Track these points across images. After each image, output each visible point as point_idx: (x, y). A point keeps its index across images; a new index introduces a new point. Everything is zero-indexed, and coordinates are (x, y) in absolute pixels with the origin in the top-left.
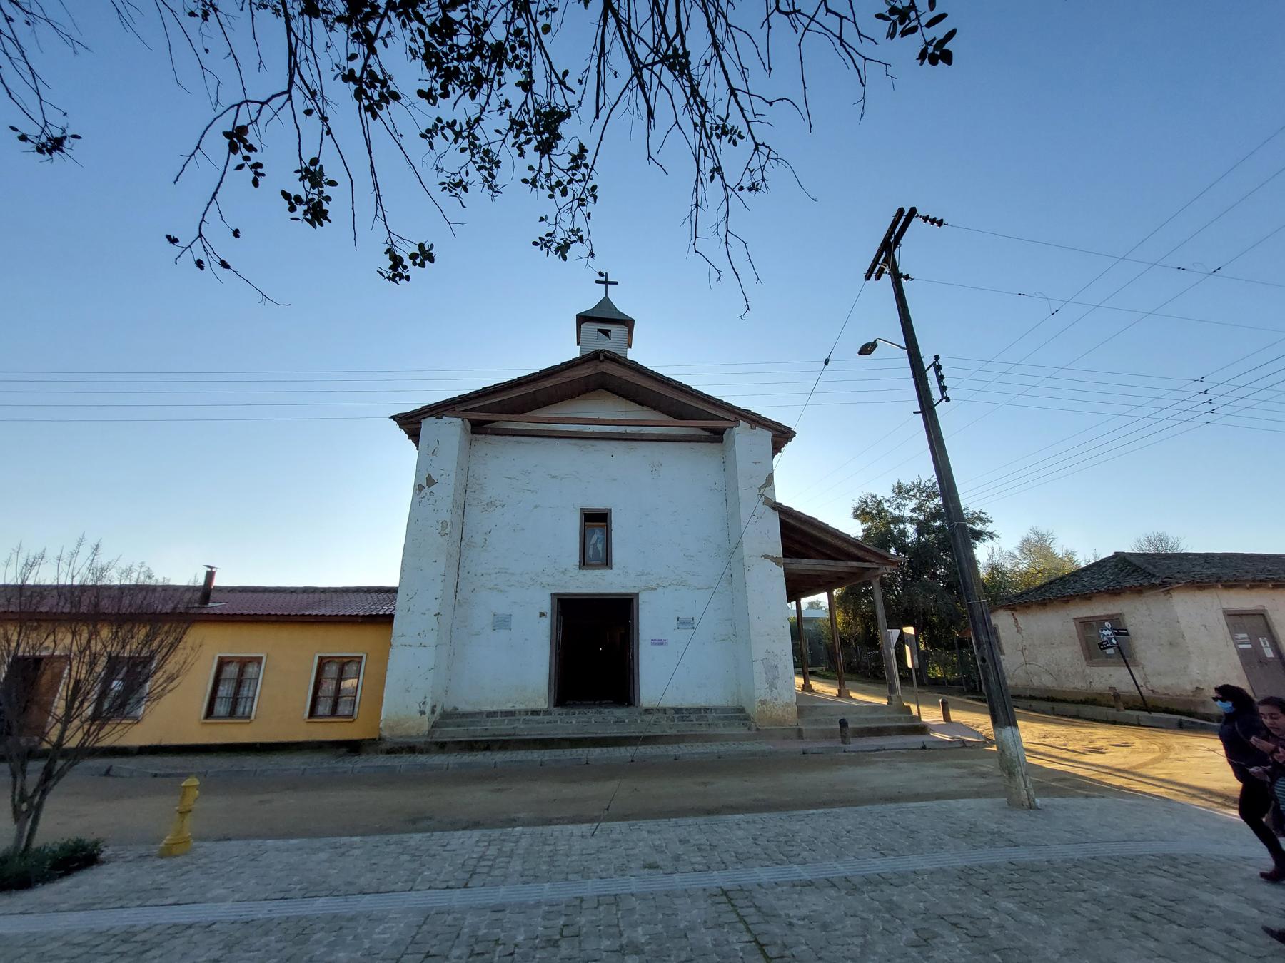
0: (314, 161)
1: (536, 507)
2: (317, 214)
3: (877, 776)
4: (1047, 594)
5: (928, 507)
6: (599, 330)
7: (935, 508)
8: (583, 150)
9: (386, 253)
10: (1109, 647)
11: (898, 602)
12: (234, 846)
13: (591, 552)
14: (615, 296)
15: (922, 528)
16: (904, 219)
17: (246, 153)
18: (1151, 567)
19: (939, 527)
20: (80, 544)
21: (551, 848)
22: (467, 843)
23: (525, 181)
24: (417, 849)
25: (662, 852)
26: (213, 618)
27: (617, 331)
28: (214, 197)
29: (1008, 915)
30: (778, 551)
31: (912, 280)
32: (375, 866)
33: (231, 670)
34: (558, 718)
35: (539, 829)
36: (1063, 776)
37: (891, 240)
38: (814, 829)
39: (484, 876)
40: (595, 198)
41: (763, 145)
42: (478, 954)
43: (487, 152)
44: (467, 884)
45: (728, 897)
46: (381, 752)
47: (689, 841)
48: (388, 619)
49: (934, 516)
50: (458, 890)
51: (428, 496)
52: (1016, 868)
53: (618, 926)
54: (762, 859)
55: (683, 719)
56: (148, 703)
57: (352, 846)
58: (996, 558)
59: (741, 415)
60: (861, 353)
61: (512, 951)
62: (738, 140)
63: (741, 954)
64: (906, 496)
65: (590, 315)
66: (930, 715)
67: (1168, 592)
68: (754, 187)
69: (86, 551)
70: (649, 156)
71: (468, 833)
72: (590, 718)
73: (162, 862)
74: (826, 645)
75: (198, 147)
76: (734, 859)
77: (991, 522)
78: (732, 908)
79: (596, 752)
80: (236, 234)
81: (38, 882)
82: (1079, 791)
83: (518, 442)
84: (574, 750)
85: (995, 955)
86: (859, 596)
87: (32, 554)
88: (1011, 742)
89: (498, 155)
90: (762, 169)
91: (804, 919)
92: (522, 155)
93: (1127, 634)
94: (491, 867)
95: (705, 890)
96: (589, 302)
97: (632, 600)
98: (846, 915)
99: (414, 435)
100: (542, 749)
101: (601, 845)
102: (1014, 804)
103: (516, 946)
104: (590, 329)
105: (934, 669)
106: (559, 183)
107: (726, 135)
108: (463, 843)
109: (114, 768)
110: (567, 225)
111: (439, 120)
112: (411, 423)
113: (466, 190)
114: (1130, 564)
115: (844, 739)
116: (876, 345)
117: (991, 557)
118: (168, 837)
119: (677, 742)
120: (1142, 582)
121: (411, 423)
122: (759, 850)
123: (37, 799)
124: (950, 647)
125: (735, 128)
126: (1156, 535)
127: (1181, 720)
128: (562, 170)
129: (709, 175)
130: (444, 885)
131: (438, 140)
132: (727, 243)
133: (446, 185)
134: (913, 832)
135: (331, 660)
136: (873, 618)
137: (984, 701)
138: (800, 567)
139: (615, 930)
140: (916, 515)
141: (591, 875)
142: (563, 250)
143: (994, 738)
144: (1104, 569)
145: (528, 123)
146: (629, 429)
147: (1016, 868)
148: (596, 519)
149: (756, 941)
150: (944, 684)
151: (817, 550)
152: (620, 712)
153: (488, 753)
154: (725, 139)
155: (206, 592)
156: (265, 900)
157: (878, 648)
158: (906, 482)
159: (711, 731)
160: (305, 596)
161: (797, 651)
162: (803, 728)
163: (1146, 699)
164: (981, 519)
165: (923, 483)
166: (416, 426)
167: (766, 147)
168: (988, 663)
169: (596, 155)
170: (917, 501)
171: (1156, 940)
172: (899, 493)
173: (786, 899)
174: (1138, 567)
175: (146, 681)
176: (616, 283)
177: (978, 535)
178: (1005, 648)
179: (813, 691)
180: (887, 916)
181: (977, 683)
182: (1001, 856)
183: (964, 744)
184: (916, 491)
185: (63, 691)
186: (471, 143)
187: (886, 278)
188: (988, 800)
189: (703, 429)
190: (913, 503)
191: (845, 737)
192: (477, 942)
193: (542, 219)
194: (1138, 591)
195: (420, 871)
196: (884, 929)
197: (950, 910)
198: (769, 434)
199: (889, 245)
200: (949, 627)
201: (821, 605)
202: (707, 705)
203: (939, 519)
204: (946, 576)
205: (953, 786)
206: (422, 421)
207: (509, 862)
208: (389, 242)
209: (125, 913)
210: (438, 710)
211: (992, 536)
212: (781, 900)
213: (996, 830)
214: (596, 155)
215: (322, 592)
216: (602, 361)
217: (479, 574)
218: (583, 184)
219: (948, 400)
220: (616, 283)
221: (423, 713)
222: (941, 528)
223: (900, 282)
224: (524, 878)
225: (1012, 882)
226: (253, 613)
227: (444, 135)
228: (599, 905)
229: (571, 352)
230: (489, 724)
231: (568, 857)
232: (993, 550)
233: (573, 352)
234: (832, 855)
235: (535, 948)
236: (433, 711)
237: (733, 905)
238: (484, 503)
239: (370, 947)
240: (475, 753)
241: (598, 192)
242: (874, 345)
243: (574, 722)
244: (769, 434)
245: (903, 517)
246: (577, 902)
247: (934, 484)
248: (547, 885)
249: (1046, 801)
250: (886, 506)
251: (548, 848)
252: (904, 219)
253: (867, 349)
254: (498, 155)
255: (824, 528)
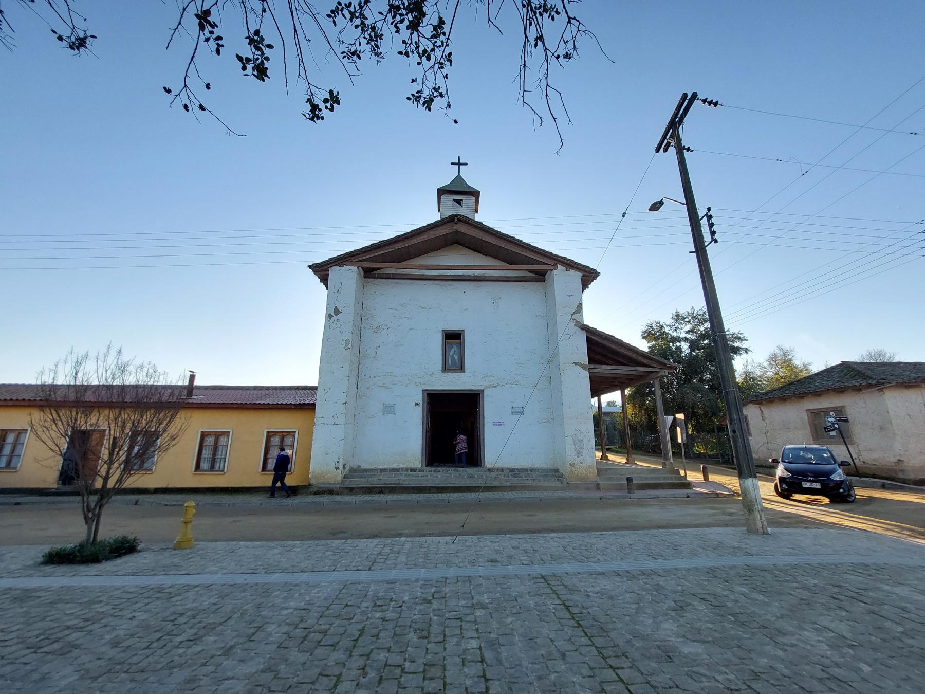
0: (257, 32)
1: (410, 329)
2: (261, 72)
3: (653, 513)
4: (787, 392)
5: (699, 330)
6: (454, 200)
7: (704, 330)
8: (441, 22)
9: (306, 102)
10: (833, 430)
11: (673, 400)
12: (219, 544)
13: (450, 361)
14: (466, 174)
15: (694, 345)
16: (686, 102)
17: (210, 29)
18: (870, 372)
19: (707, 344)
20: (109, 349)
21: (425, 549)
22: (370, 546)
23: (400, 53)
24: (337, 549)
25: (500, 553)
26: (196, 406)
27: (468, 200)
28: (192, 59)
29: (742, 594)
30: (585, 360)
31: (692, 151)
32: (310, 558)
33: (210, 440)
34: (429, 474)
35: (417, 539)
36: (789, 515)
37: (677, 120)
38: (606, 543)
39: (381, 564)
40: (451, 61)
41: (574, 18)
42: (379, 606)
43: (373, 29)
44: (370, 568)
45: (545, 580)
46: (311, 493)
47: (518, 548)
48: (312, 407)
49: (703, 336)
50: (364, 572)
51: (336, 322)
52: (749, 568)
53: (470, 593)
54: (569, 559)
55: (515, 476)
56: (160, 453)
57: (294, 546)
58: (749, 368)
59: (559, 261)
60: (651, 210)
61: (400, 605)
62: (555, 15)
63: (554, 611)
64: (683, 322)
65: (447, 189)
66: (694, 477)
67: (881, 390)
68: (567, 56)
69: (113, 353)
70: (489, 20)
71: (370, 540)
72: (451, 474)
73: (177, 552)
74: (619, 430)
75: (180, 23)
76: (550, 558)
77: (747, 340)
78: (547, 586)
79: (455, 496)
80: (208, 86)
81: (103, 559)
82: (801, 525)
83: (397, 283)
84: (440, 494)
85: (730, 617)
86: (644, 396)
87: (80, 355)
88: (751, 488)
89: (381, 30)
90: (574, 39)
91: (597, 593)
92: (397, 32)
93: (847, 421)
94: (386, 559)
95: (529, 575)
96: (446, 180)
97: (479, 394)
98: (626, 592)
99: (324, 280)
100: (417, 493)
101: (458, 548)
102: (751, 530)
103: (403, 602)
104: (448, 199)
105: (698, 447)
106: (425, 51)
107: (547, 12)
108: (367, 545)
109: (140, 501)
110: (430, 84)
111: (339, 3)
112: (322, 270)
113: (359, 58)
114: (853, 369)
115: (630, 490)
116: (663, 203)
117: (746, 367)
118: (178, 538)
119: (512, 491)
120: (862, 382)
121: (322, 270)
122: (567, 554)
123: (97, 511)
124: (711, 431)
125: (553, 6)
126: (876, 350)
127: (884, 482)
128: (427, 38)
129: (533, 43)
130: (355, 568)
131: (339, 18)
132: (547, 95)
133: (345, 54)
134: (676, 546)
135: (275, 433)
136: (654, 410)
137: (735, 469)
138: (601, 371)
139: (469, 595)
140: (690, 336)
141: (452, 565)
142: (428, 103)
143: (740, 492)
144: (832, 374)
145: (402, 6)
146: (477, 273)
147: (749, 568)
148: (453, 338)
149: (565, 605)
150: (705, 457)
151: (613, 360)
152: (471, 470)
153: (382, 495)
154: (546, 15)
155: (190, 389)
156: (242, 573)
157: (657, 431)
158: (683, 311)
159: (535, 484)
160: (256, 392)
161: (598, 435)
162: (601, 482)
163: (858, 469)
164: (739, 338)
165: (695, 312)
166: (325, 273)
167: (576, 20)
168: (738, 433)
169: (451, 28)
170: (691, 326)
171: (847, 611)
172: (677, 320)
173: (586, 582)
174: (860, 372)
175: (157, 439)
176: (466, 164)
177: (736, 350)
178: (752, 431)
179: (609, 460)
180: (655, 593)
181: (730, 457)
182: (739, 561)
183: (718, 495)
184: (690, 318)
185: (106, 443)
186: (362, 23)
187: (672, 150)
188: (733, 529)
189: (530, 271)
190: (688, 327)
191: (631, 489)
192: (378, 599)
193: (413, 81)
194: (858, 389)
195: (339, 560)
196: (652, 600)
197: (701, 591)
198: (579, 274)
199: (675, 124)
200: (711, 417)
201: (616, 404)
202: (533, 467)
203: (707, 339)
204: (711, 380)
205: (708, 520)
206: (330, 269)
207: (398, 557)
208: (309, 93)
209: (157, 578)
210: (348, 468)
211: (746, 351)
212: (582, 582)
213: (737, 546)
214: (451, 28)
215: (267, 389)
216: (456, 223)
217: (372, 376)
218: (442, 49)
219: (716, 241)
220: (466, 164)
221: (337, 468)
222: (709, 345)
223: (683, 152)
224: (408, 566)
225: (746, 576)
226: (222, 402)
227: (343, 15)
228: (458, 581)
229: (434, 216)
230: (382, 477)
231: (437, 554)
232: (747, 361)
233: (435, 217)
234: (618, 558)
235: (416, 604)
236: (344, 468)
237: (548, 584)
238: (375, 327)
239: (310, 600)
240: (373, 495)
241: (453, 58)
242: (661, 203)
243: (439, 476)
244: (579, 274)
245: (679, 337)
246: (444, 580)
247: (704, 313)
248: (423, 570)
249: (776, 530)
250: (667, 329)
251: (423, 550)
252: (686, 102)
253: (656, 207)
254: (381, 30)
255: (620, 343)
